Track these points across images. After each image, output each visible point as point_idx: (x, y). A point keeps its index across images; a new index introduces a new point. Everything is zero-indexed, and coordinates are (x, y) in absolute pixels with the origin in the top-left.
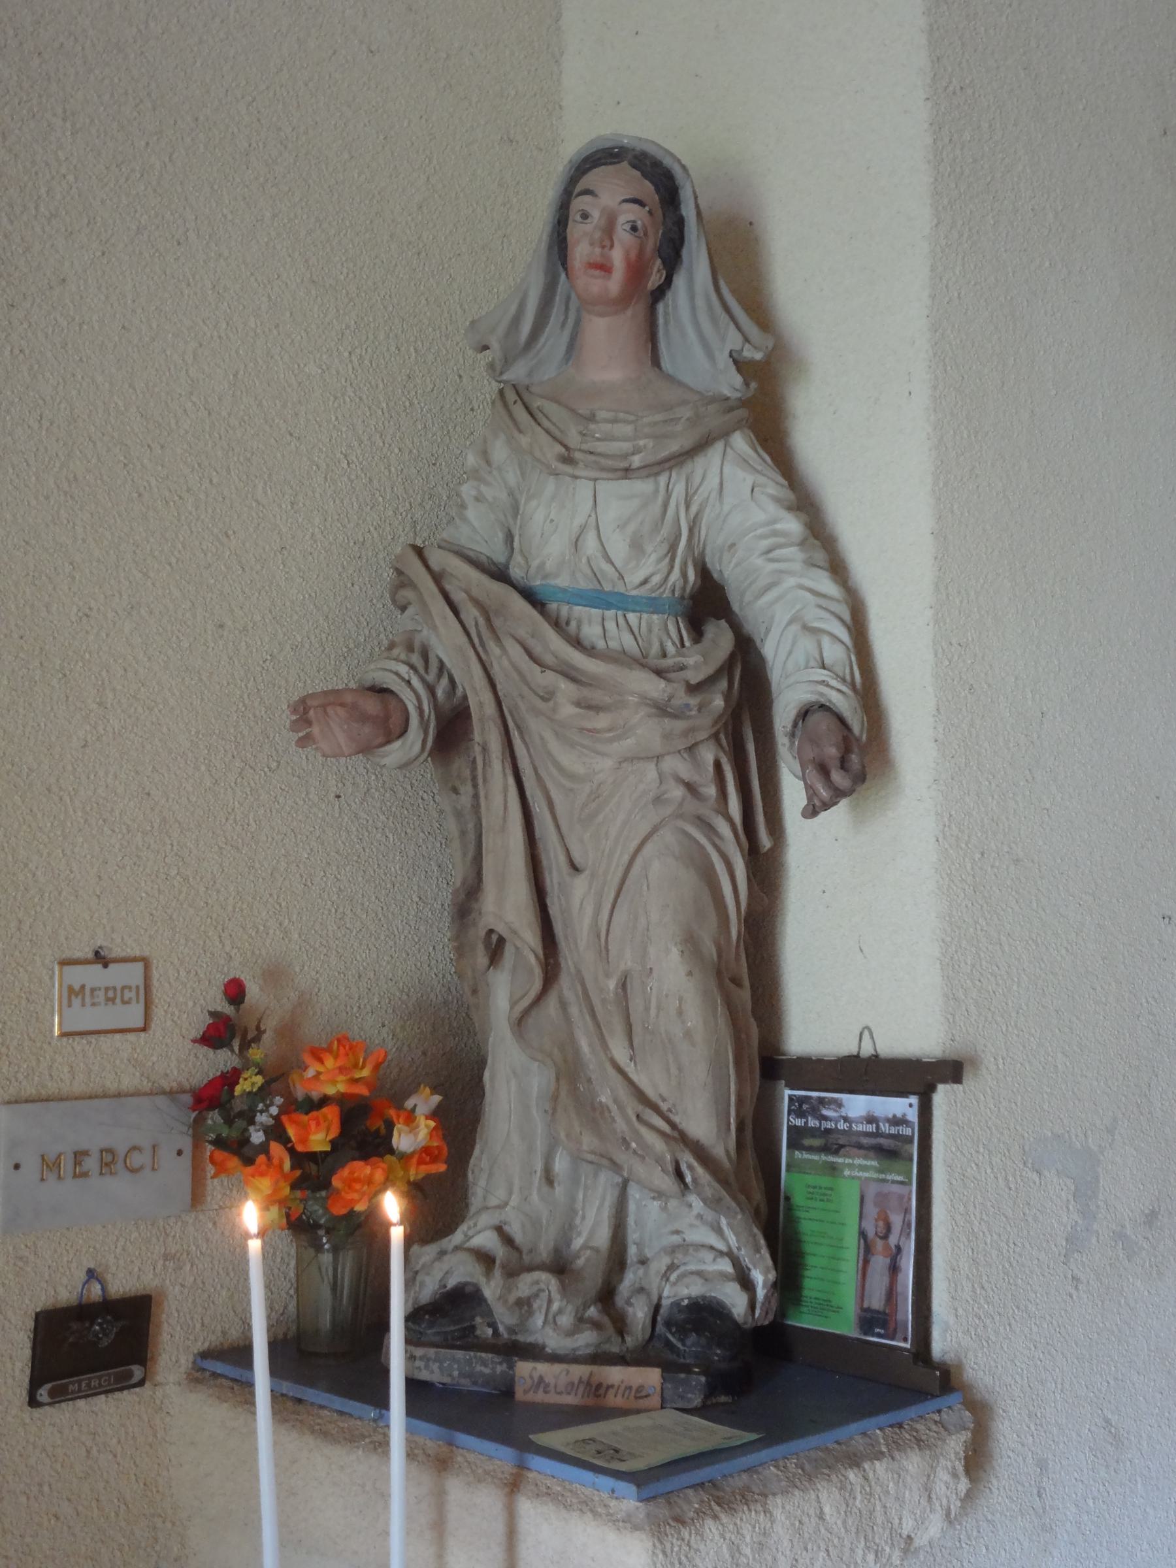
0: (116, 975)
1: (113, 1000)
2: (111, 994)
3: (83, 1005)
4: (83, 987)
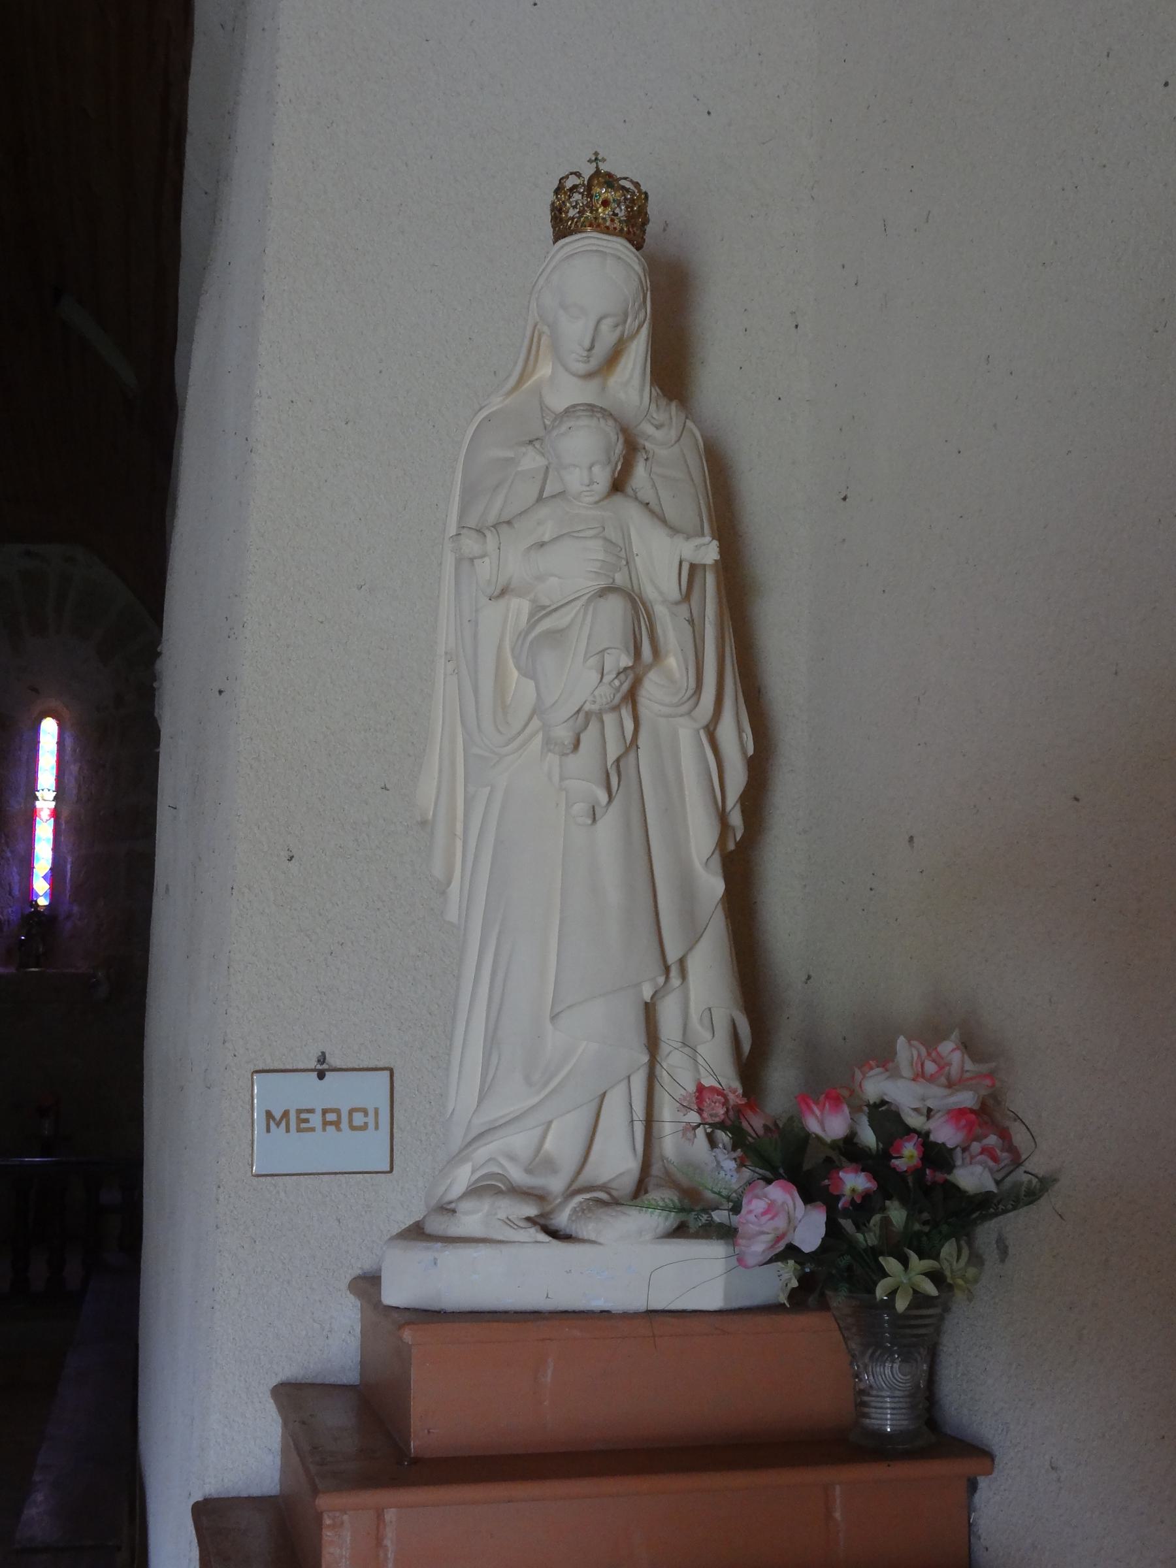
0: (339, 1092)
1: (337, 1124)
2: (331, 1117)
3: (288, 1130)
4: (286, 1114)
